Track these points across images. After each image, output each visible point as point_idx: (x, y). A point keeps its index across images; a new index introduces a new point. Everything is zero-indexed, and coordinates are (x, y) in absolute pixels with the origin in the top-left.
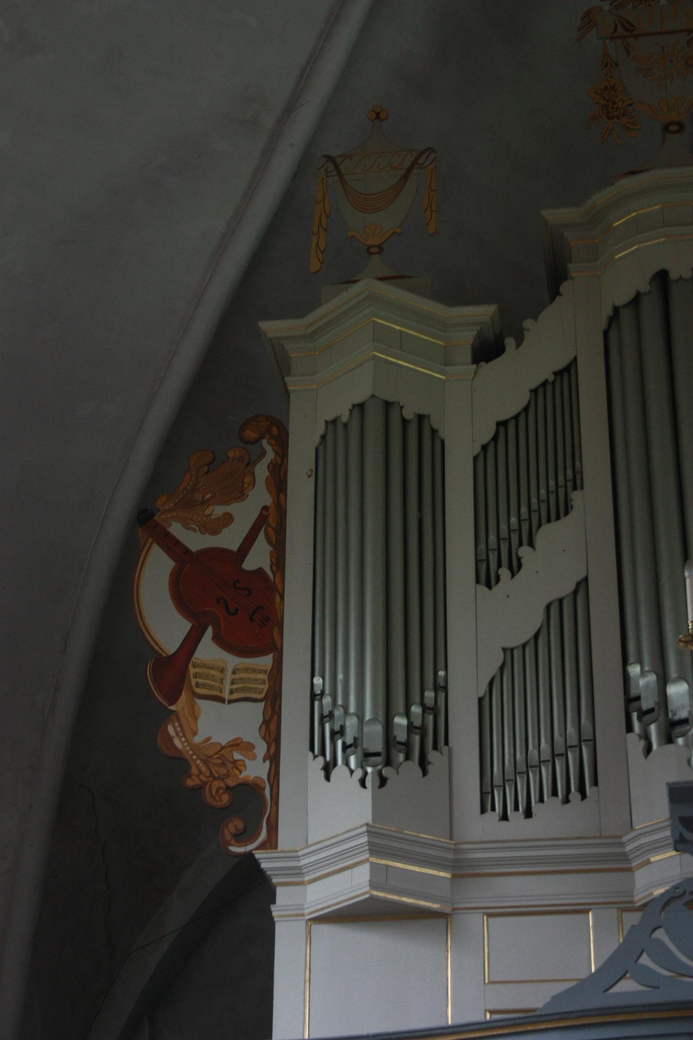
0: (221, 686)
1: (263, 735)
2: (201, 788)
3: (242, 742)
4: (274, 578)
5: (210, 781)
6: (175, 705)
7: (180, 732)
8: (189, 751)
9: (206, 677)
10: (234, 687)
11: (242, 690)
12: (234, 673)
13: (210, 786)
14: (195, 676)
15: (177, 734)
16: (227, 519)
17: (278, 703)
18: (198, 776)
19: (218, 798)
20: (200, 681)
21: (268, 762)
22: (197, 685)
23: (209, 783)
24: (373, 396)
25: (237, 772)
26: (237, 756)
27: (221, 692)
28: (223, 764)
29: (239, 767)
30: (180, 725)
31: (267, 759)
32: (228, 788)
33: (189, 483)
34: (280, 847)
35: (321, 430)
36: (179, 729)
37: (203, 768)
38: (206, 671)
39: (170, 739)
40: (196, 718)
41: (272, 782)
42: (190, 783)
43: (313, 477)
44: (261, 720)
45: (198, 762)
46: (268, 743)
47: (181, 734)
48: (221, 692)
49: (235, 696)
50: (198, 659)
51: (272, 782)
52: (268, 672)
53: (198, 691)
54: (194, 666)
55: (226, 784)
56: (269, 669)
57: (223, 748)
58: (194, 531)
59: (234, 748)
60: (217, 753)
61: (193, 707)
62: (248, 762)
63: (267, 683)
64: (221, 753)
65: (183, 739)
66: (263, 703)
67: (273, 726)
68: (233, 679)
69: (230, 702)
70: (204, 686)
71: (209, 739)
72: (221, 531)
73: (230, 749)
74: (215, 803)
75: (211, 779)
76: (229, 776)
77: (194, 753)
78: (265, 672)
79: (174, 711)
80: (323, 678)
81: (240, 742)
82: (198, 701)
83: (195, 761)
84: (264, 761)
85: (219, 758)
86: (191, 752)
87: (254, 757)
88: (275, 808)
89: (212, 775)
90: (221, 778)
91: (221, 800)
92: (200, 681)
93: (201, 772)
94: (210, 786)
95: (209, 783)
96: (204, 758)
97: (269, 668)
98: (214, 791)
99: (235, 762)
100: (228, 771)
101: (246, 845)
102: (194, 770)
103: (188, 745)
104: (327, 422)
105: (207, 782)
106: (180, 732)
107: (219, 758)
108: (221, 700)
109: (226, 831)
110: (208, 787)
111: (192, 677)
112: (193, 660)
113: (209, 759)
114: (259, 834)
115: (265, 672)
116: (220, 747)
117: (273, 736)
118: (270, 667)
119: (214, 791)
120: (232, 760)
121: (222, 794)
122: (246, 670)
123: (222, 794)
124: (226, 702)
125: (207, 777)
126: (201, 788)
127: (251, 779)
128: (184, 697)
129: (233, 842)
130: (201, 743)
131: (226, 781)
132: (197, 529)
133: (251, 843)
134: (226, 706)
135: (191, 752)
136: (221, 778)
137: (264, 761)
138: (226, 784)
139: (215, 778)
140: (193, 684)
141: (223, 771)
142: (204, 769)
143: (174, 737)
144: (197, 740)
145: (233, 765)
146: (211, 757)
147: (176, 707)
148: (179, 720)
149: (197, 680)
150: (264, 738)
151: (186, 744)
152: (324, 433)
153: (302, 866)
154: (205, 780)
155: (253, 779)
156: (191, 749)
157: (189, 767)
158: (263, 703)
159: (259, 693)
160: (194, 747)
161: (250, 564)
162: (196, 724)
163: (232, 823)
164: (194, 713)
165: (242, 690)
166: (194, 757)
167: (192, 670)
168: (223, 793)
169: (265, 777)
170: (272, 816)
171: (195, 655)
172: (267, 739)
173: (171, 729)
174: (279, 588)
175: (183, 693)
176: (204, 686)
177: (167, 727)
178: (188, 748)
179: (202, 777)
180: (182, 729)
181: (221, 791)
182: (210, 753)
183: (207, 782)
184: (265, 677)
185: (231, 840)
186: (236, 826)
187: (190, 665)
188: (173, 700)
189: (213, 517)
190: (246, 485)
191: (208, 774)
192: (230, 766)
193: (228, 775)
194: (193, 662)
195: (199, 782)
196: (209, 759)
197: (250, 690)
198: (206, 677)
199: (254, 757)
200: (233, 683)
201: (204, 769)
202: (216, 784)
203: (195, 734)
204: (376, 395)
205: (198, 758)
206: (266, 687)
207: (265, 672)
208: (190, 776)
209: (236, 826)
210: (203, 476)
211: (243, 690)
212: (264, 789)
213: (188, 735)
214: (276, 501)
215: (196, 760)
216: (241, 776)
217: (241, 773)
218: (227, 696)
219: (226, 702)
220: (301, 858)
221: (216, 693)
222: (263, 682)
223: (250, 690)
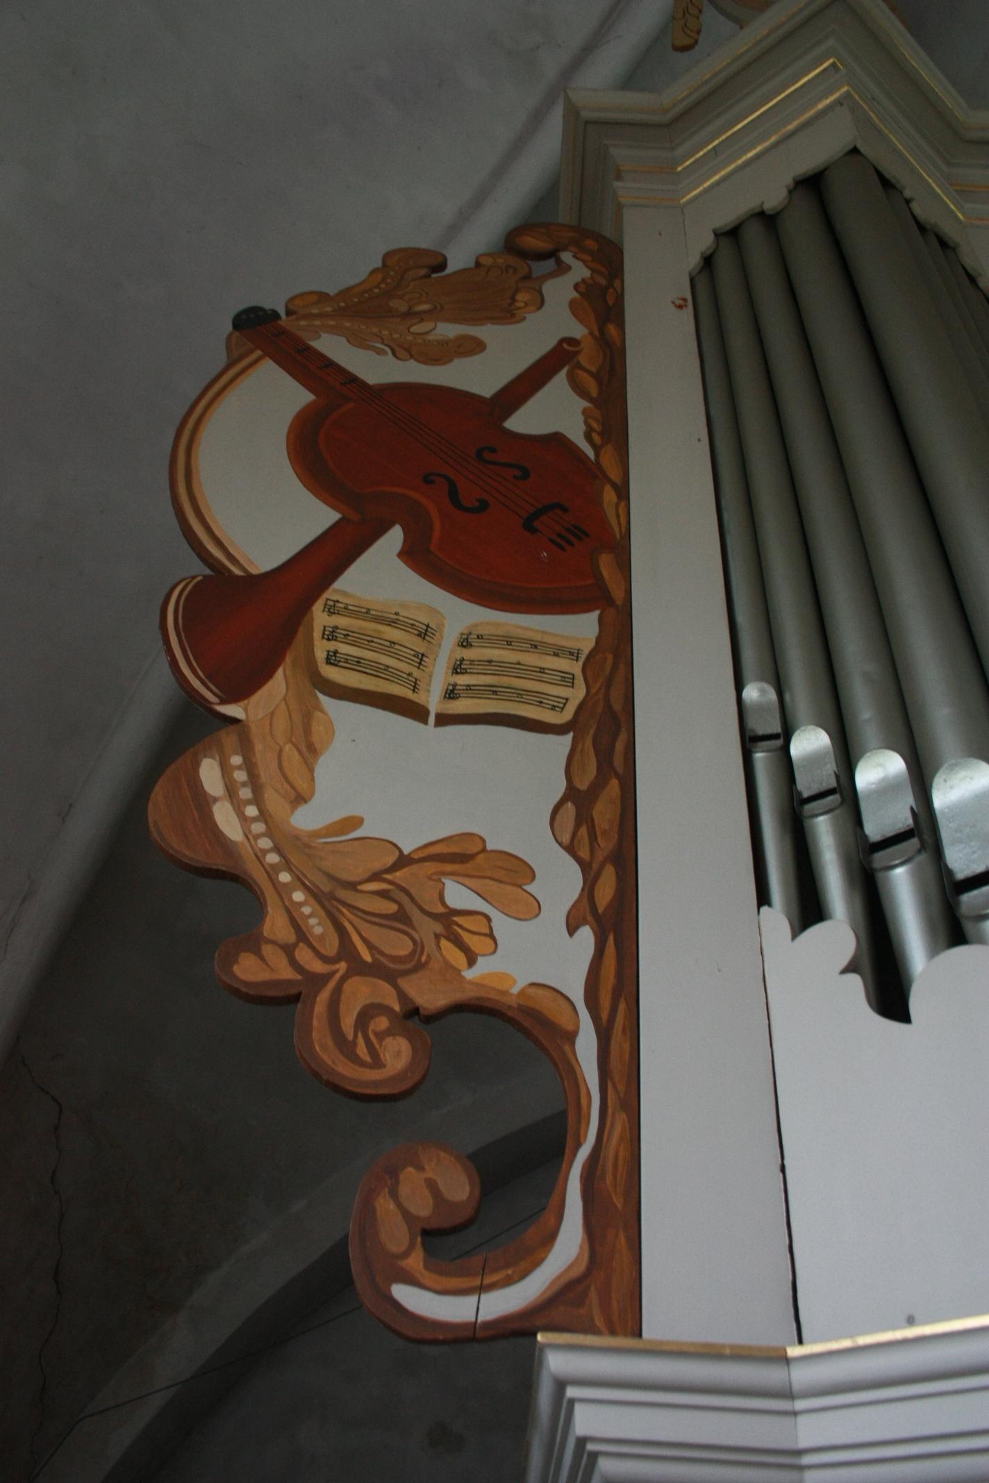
0: (416, 673)
1: (566, 839)
2: (296, 998)
3: (484, 850)
4: (597, 455)
5: (338, 976)
6: (242, 704)
7: (244, 784)
8: (265, 852)
9: (368, 642)
10: (462, 680)
11: (493, 691)
12: (465, 643)
13: (338, 991)
14: (331, 634)
15: (231, 790)
16: (474, 347)
17: (619, 747)
18: (289, 950)
19: (362, 1050)
20: (344, 649)
21: (586, 935)
22: (332, 659)
23: (332, 984)
24: (855, 151)
25: (458, 958)
26: (458, 895)
27: (414, 689)
28: (401, 919)
29: (466, 937)
30: (250, 766)
31: (584, 922)
32: (413, 1013)
33: (290, 870)
34: (654, 1326)
35: (705, 241)
36: (241, 776)
37: (313, 921)
38: (370, 626)
39: (203, 803)
40: (310, 751)
41: (605, 1015)
42: (248, 969)
43: (690, 309)
44: (559, 786)
45: (298, 896)
46: (584, 866)
47: (245, 793)
48: (414, 689)
49: (462, 706)
50: (345, 594)
51: (605, 1015)
52: (583, 657)
53: (332, 673)
54: (331, 610)
55: (402, 996)
56: (586, 651)
57: (404, 861)
58: (380, 352)
59: (449, 867)
60: (376, 877)
61: (307, 718)
62: (501, 924)
63: (580, 681)
64: (398, 876)
65: (251, 811)
66: (570, 736)
67: (605, 812)
68: (462, 660)
69: (444, 720)
70: (357, 664)
71: (354, 822)
72: (451, 361)
73: (431, 867)
74: (345, 1070)
75: (342, 967)
76: (419, 967)
77: (288, 866)
78: (574, 654)
79: (234, 721)
80: (780, 685)
81: (474, 849)
82: (324, 700)
83: (271, 872)
84: (572, 930)
85: (383, 894)
86: (273, 858)
87: (533, 909)
88: (619, 1123)
89: (346, 950)
90: (381, 970)
91: (377, 1063)
92: (344, 649)
93: (302, 935)
94: (338, 991)
95: (332, 984)
96: (325, 886)
97: (587, 647)
98: (348, 1022)
99: (448, 917)
100: (418, 946)
101: (482, 1289)
102: (276, 925)
103: (269, 834)
104: (718, 235)
105: (326, 978)
106: (244, 784)
107: (383, 894)
108: (417, 712)
109: (385, 1205)
110: (324, 996)
111: (317, 634)
112: (328, 594)
113: (342, 894)
114: (550, 1238)
115: (574, 654)
116: (390, 860)
117: (606, 845)
118: (592, 644)
119: (348, 1022)
120: (441, 910)
121: (381, 1036)
122: (508, 642)
123: (381, 1036)
124: (432, 719)
125: (325, 959)
126: (296, 998)
127: (515, 990)
128: (278, 685)
129: (415, 1261)
130: (316, 834)
131: (402, 982)
132: (389, 351)
133: (508, 1282)
134: (429, 730)
135: (273, 858)
136: (381, 970)
137: (572, 930)
138: (402, 996)
139: (358, 968)
140: (320, 655)
141: (397, 945)
142: (317, 926)
143: (216, 800)
144: (305, 819)
145: (438, 928)
146: (352, 886)
147: (246, 710)
148: (246, 747)
149: (332, 646)
150: (570, 849)
151: (258, 828)
152: (711, 251)
153: (800, 1453)
154: (318, 967)
155: (522, 992)
156: (277, 849)
157: (258, 908)
158: (570, 736)
159: (553, 708)
160: (288, 843)
161: (526, 421)
162: (311, 770)
163: (421, 1168)
164: (307, 732)
165: (493, 691)
166: (285, 877)
167: (320, 618)
168: (389, 1033)
169: (576, 992)
170: (611, 1153)
171: (337, 585)
172: (584, 854)
173: (209, 774)
174: (614, 474)
175: (280, 673)
176: (357, 664)
177: (196, 765)
178: (265, 843)
179: (304, 955)
180: (254, 781)
181: (382, 1023)
182: (353, 869)
183: (325, 978)
184: (576, 668)
185: (406, 1254)
186: (432, 1185)
187: (318, 607)
188: (240, 690)
189: (430, 337)
190: (518, 304)
191: (332, 946)
192: (427, 928)
193: (416, 964)
194: (327, 599)
195: (286, 972)
196: (342, 894)
197: (520, 695)
198: (368, 642)
199: (533, 909)
200: (458, 669)
201: (317, 926)
202: (360, 992)
203: (299, 799)
204: (862, 149)
205: (300, 881)
206: (577, 694)
207: (571, 654)
208: (254, 943)
209: (432, 1185)
210: (414, 280)
211: (495, 693)
212: (571, 1037)
213: (274, 801)
214: (596, 333)
215: (289, 888)
216: (469, 974)
217: (471, 961)
218: (434, 701)
219: (432, 719)
220: (800, 1405)
221: (407, 693)
222: (567, 679)
223: (520, 695)
